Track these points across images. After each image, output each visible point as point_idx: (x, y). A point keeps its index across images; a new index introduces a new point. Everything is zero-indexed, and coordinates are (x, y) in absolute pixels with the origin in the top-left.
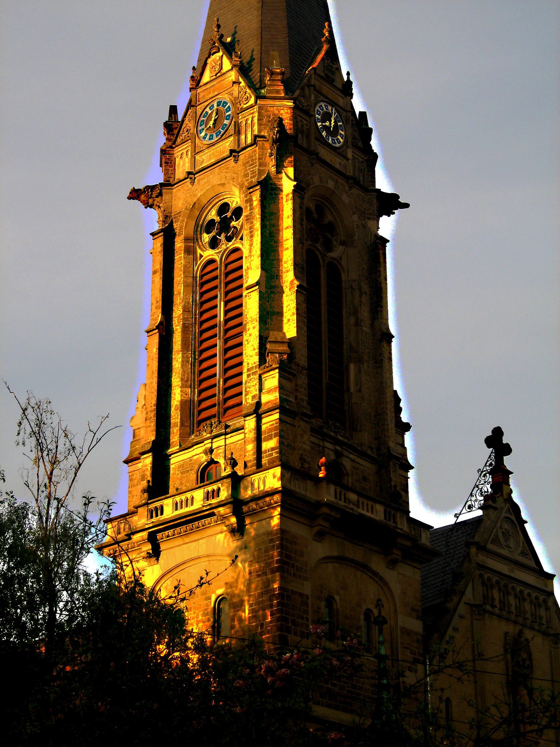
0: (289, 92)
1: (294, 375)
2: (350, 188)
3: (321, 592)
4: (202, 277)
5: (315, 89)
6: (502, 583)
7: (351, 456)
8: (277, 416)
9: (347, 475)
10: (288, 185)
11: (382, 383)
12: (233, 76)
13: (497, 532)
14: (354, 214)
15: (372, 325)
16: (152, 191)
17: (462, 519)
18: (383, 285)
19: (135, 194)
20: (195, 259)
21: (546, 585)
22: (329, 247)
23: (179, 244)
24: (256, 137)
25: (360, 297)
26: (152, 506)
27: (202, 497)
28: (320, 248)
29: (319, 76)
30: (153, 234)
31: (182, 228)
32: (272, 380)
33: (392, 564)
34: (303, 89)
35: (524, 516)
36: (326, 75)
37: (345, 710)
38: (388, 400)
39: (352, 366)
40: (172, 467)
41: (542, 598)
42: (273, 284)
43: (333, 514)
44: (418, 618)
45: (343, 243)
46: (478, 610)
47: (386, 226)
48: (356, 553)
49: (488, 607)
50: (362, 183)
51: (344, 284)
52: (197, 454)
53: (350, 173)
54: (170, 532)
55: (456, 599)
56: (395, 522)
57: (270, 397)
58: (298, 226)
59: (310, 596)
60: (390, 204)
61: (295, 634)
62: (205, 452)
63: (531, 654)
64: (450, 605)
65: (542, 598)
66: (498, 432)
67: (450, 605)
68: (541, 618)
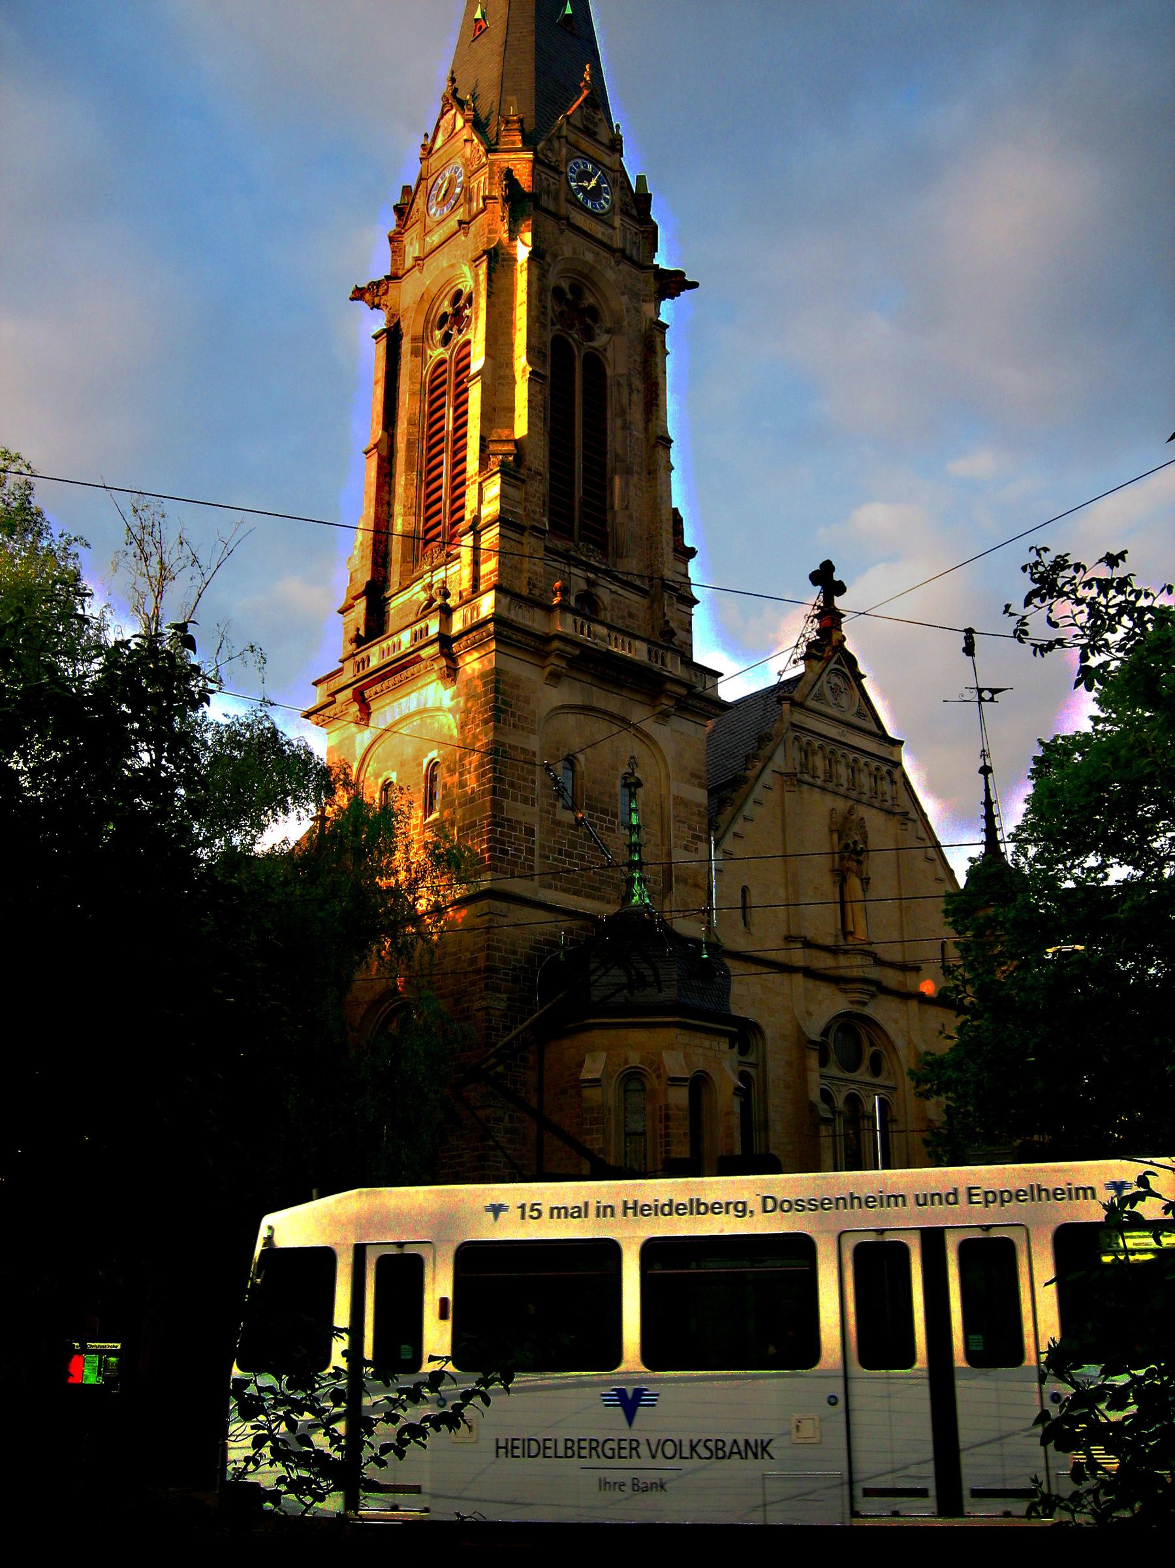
0: (529, 143)
1: (523, 481)
2: (618, 263)
3: (558, 750)
4: (432, 381)
5: (567, 141)
6: (828, 749)
7: (611, 587)
8: (497, 530)
9: (605, 609)
10: (522, 252)
11: (656, 497)
12: (465, 134)
13: (822, 686)
14: (623, 294)
15: (646, 429)
16: (378, 288)
17: (786, 677)
18: (660, 380)
19: (359, 294)
20: (424, 363)
21: (892, 754)
22: (589, 335)
23: (406, 345)
24: (485, 198)
25: (630, 394)
26: (358, 658)
27: (409, 638)
28: (576, 336)
29: (575, 126)
30: (375, 337)
31: (410, 328)
32: (494, 487)
33: (664, 716)
34: (549, 140)
35: (862, 669)
36: (585, 127)
37: (588, 896)
38: (664, 518)
39: (617, 481)
40: (392, 612)
41: (885, 769)
42: (502, 373)
43: (568, 649)
44: (701, 786)
45: (608, 331)
46: (793, 779)
47: (667, 310)
48: (612, 703)
49: (807, 778)
50: (635, 257)
51: (608, 381)
52: (417, 593)
53: (618, 243)
54: (378, 687)
55: (759, 765)
56: (663, 664)
57: (491, 509)
58: (535, 302)
59: (538, 753)
60: (673, 284)
61: (515, 799)
62: (424, 589)
63: (867, 837)
64: (751, 774)
65: (885, 769)
66: (828, 567)
67: (751, 774)
68: (884, 794)
